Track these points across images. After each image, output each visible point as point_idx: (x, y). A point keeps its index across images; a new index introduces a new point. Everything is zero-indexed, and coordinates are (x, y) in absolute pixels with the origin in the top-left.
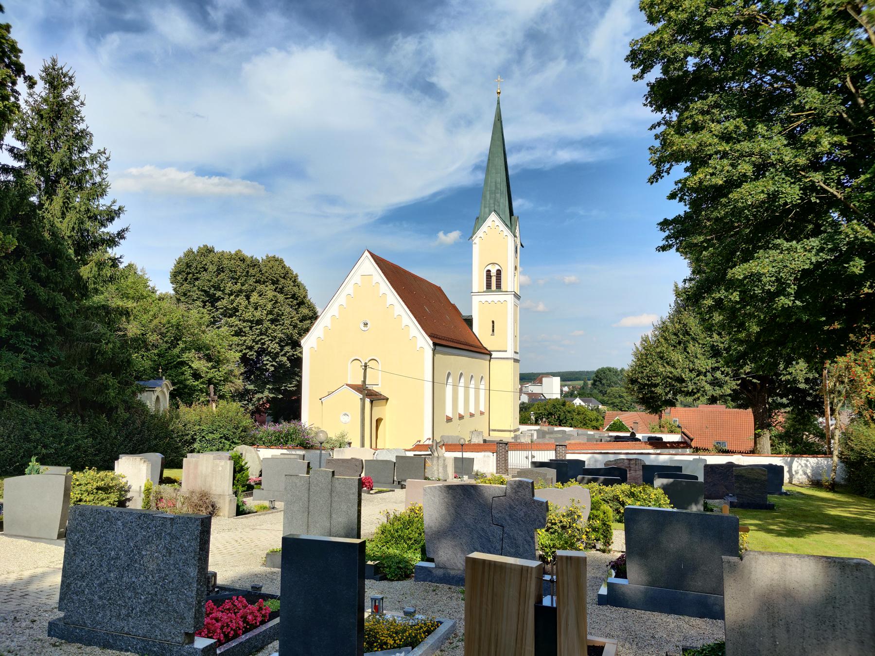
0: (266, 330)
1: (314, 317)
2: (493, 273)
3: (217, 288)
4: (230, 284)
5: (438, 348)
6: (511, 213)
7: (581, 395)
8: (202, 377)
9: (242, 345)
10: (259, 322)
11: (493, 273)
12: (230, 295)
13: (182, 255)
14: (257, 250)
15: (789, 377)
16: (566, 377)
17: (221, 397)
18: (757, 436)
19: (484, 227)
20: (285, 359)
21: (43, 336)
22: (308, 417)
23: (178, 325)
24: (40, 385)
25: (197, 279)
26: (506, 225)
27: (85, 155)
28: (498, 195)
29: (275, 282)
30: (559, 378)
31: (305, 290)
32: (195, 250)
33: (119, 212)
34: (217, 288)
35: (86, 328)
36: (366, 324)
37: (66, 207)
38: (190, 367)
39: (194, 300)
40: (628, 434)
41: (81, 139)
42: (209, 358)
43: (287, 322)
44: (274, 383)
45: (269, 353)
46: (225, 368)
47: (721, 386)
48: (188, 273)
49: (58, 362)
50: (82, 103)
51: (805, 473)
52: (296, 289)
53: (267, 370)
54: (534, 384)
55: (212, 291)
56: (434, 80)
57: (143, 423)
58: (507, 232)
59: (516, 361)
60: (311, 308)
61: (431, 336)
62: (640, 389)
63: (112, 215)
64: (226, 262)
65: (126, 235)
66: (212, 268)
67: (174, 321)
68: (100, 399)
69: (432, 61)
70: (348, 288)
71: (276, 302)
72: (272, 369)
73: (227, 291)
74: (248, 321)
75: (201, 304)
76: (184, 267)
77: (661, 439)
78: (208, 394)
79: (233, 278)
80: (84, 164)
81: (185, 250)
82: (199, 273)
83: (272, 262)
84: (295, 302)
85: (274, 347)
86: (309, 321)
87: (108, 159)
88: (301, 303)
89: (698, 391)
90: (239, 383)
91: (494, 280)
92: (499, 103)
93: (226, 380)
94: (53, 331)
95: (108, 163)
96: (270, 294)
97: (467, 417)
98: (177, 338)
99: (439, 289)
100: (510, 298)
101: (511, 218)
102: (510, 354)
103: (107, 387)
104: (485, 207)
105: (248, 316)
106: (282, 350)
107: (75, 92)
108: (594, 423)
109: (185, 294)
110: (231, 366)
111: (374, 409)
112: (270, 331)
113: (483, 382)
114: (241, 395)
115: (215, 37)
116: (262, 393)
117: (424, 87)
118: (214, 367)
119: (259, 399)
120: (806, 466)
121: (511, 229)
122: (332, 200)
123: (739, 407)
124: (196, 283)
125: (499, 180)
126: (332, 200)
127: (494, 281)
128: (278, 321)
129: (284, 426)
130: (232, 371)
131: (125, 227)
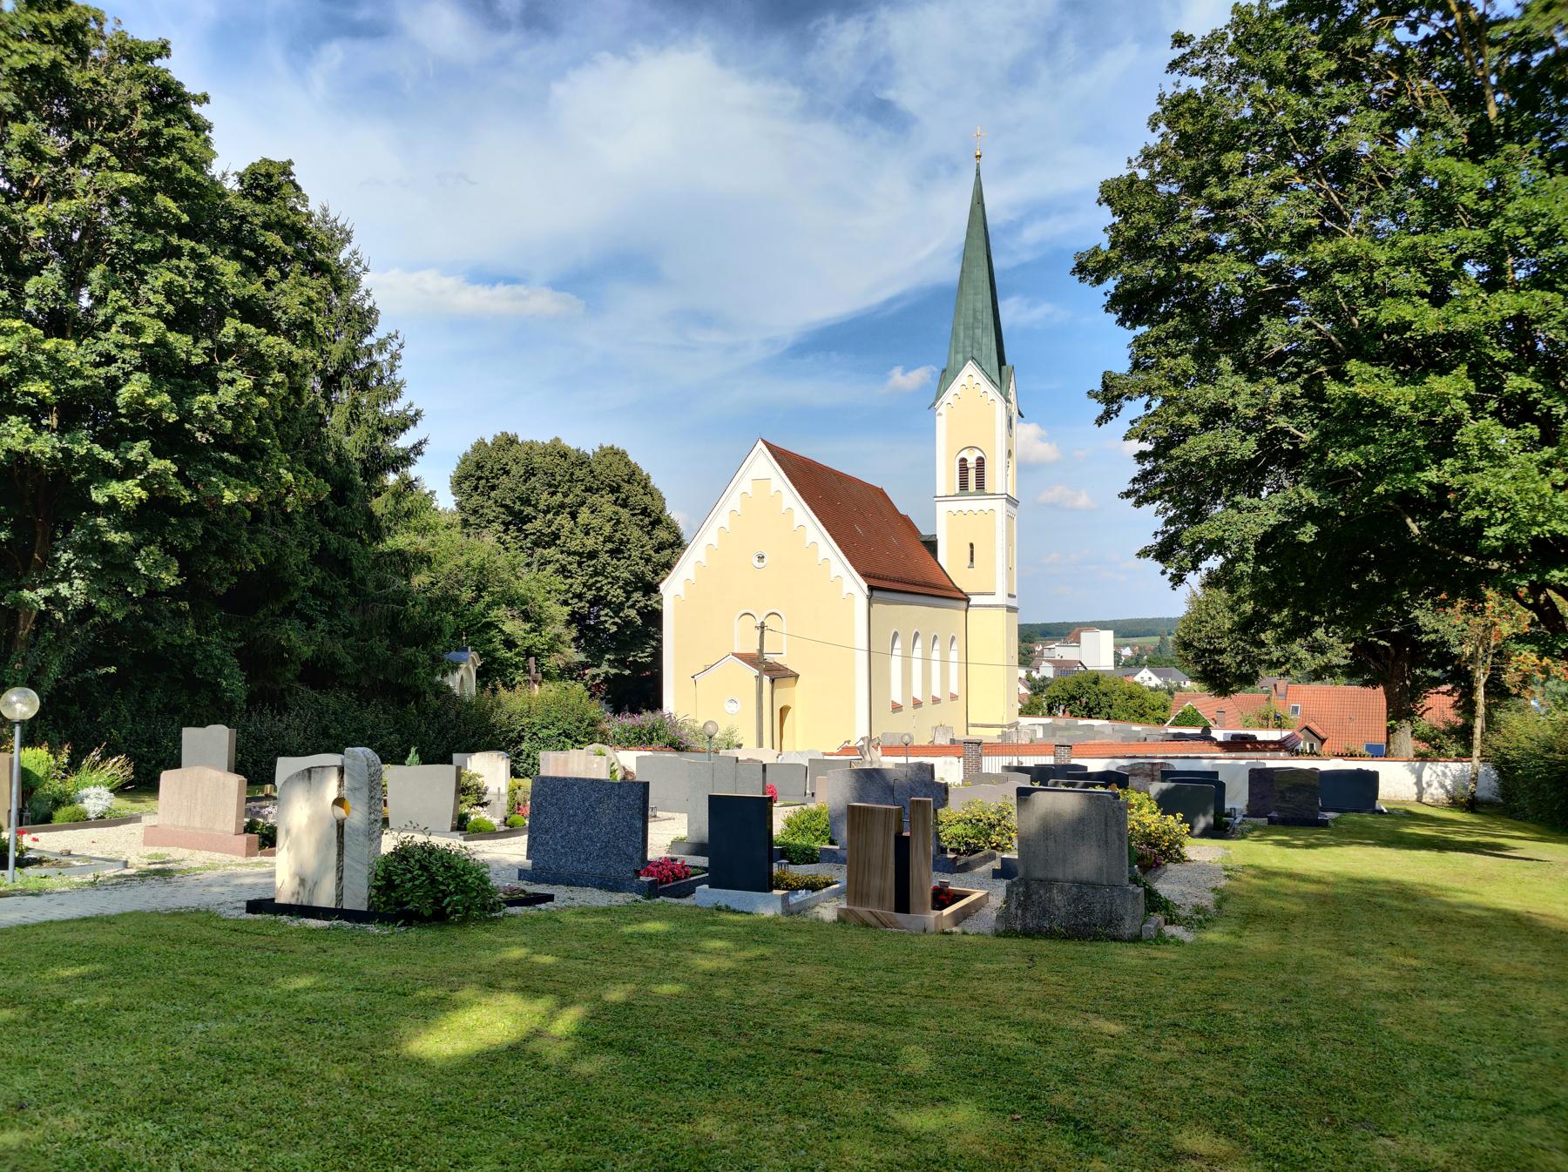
0: (604, 567)
1: (677, 544)
2: (971, 463)
3: (526, 501)
4: (545, 496)
5: (876, 594)
6: (1001, 361)
7: (1152, 664)
8: (516, 646)
9: (567, 591)
10: (593, 555)
11: (971, 463)
12: (546, 512)
13: (469, 449)
14: (584, 440)
15: (1433, 637)
16: (1124, 631)
17: (546, 675)
18: (1391, 730)
19: (955, 387)
20: (633, 613)
21: (333, 597)
22: (673, 700)
23: (483, 567)
24: (337, 664)
25: (493, 488)
26: (993, 382)
27: (368, 340)
28: (979, 332)
29: (615, 490)
30: (1111, 633)
31: (662, 500)
32: (489, 441)
33: (414, 419)
34: (526, 501)
35: (381, 585)
36: (761, 558)
37: (354, 417)
38: (501, 631)
39: (489, 522)
40: (1198, 731)
41: (363, 320)
42: (526, 617)
43: (636, 554)
44: (616, 651)
45: (608, 604)
46: (550, 631)
47: (1323, 653)
48: (480, 478)
49: (351, 632)
50: (366, 269)
51: (1442, 786)
52: (647, 499)
53: (605, 630)
54: (1066, 644)
55: (517, 507)
56: (890, 94)
57: (458, 714)
58: (993, 393)
59: (1011, 609)
60: (672, 528)
61: (865, 576)
62: (1198, 659)
63: (407, 422)
64: (537, 459)
65: (425, 449)
66: (517, 470)
67: (475, 563)
68: (404, 681)
69: (889, 60)
70: (732, 500)
71: (618, 522)
72: (614, 629)
73: (541, 507)
74: (575, 553)
75: (501, 528)
76: (471, 469)
77: (1254, 737)
78: (528, 672)
79: (550, 486)
80: (370, 355)
81: (474, 441)
82: (496, 477)
83: (609, 457)
84: (647, 521)
85: (616, 594)
86: (669, 551)
87: (401, 346)
88: (657, 522)
89: (1288, 660)
90: (575, 656)
91: (972, 475)
92: (978, 174)
93: (551, 649)
94: (344, 591)
95: (401, 352)
96: (609, 509)
97: (927, 703)
98: (480, 588)
99: (881, 492)
100: (1000, 506)
101: (1000, 368)
102: (1001, 598)
103: (415, 665)
104: (957, 352)
105: (574, 545)
106: (628, 599)
107: (355, 253)
108: (1159, 713)
109: (475, 512)
110: (559, 628)
111: (777, 691)
112: (610, 569)
113: (955, 646)
114: (570, 672)
115: (507, 40)
116: (598, 666)
117: (873, 110)
118: (533, 630)
119: (594, 677)
120: (1444, 774)
121: (1000, 389)
122: (705, 319)
123: (1365, 684)
124: (493, 494)
125: (979, 305)
126: (705, 319)
127: (972, 476)
128: (622, 552)
129: (647, 718)
130: (559, 636)
131: (422, 438)
